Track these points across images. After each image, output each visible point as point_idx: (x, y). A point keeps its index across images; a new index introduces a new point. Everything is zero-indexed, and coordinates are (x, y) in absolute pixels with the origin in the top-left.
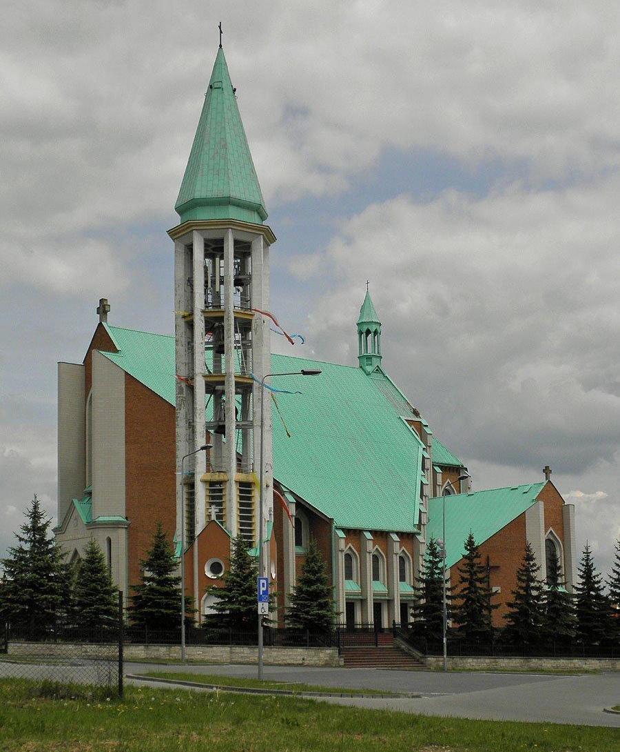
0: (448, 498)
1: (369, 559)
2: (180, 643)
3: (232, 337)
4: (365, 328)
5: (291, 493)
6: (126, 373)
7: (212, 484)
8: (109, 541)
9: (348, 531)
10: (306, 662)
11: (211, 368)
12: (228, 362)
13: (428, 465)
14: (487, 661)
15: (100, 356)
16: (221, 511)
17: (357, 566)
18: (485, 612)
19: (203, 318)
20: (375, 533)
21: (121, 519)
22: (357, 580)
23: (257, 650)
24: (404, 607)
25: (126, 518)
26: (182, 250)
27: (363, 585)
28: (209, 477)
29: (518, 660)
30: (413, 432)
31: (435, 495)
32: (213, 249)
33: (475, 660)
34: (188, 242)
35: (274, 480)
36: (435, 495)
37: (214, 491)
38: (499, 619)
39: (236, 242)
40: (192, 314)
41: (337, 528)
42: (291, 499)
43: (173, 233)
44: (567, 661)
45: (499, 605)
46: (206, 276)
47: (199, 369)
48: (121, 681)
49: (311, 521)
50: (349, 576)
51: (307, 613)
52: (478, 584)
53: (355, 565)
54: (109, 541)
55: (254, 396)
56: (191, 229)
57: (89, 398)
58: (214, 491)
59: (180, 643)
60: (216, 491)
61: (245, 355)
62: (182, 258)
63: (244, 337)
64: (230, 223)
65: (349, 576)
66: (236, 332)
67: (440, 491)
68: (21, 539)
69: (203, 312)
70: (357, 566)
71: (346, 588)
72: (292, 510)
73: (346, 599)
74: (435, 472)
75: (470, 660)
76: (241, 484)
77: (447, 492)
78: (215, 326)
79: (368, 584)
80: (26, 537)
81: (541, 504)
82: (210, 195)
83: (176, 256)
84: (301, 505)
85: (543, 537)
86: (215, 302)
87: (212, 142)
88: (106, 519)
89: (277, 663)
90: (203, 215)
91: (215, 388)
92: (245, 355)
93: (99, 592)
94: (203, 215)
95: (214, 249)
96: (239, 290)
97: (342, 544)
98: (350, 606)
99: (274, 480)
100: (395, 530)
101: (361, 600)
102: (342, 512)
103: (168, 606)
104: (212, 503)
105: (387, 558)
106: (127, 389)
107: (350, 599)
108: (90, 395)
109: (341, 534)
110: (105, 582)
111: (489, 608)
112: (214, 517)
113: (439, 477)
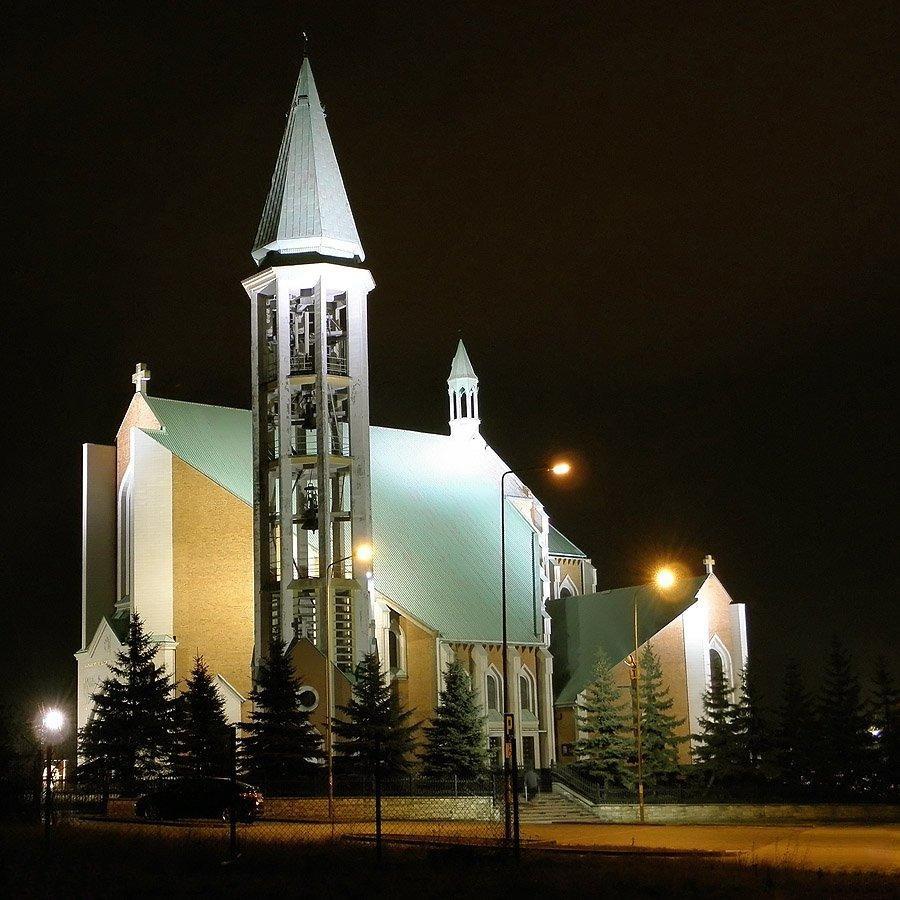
22: (534, 709)
59: (329, 796)
68: (119, 672)
80: (123, 668)
111: (675, 741)
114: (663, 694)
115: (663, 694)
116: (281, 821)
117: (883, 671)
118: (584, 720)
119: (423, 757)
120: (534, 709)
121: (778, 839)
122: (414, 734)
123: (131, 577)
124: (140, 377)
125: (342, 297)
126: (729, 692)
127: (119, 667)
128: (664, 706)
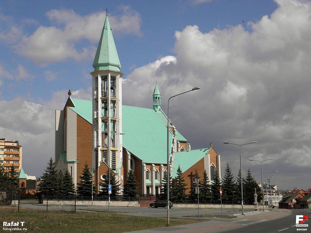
0: (182, 152)
1: (154, 173)
2: (91, 200)
3: (110, 105)
4: (155, 96)
5: (129, 152)
6: (77, 114)
7: (103, 151)
8: (71, 167)
9: (147, 164)
10: (129, 206)
11: (104, 115)
12: (108, 113)
13: (175, 141)
14: (184, 205)
15: (69, 108)
16: (106, 159)
17: (150, 175)
18: (184, 191)
19: (101, 100)
20: (156, 164)
21: (75, 160)
22: (150, 179)
23: (108, 202)
24: (157, 188)
25: (77, 160)
26: (94, 79)
27: (152, 181)
28: (102, 149)
29: (193, 205)
30: (170, 131)
31: (178, 151)
32: (104, 78)
33: (180, 205)
34: (96, 76)
35: (123, 147)
36: (178, 151)
37: (104, 153)
38: (187, 192)
39: (111, 76)
40: (98, 98)
41: (143, 163)
42: (129, 154)
43: (92, 73)
44: (209, 205)
45: (188, 189)
46: (102, 87)
47: (100, 116)
48: (75, 210)
49: (136, 161)
50: (147, 178)
51: (129, 191)
52: (181, 182)
53: (150, 174)
54: (71, 167)
55: (117, 123)
56: (97, 73)
57: (65, 121)
58: (104, 153)
59: (91, 200)
60: (105, 153)
61: (114, 111)
62: (94, 81)
63: (114, 105)
64: (109, 71)
65: (147, 178)
66: (111, 103)
67: (179, 150)
68: (47, 171)
69: (101, 98)
70: (150, 175)
71: (147, 182)
72: (129, 157)
73: (155, 185)
74: (178, 144)
75: (179, 205)
76: (112, 151)
77: (182, 150)
78: (105, 101)
79: (154, 181)
80: (48, 170)
81: (209, 155)
82: (103, 62)
83: (93, 80)
84: (132, 156)
85: (210, 165)
86: (105, 94)
87: (104, 46)
88: (71, 160)
89: (120, 206)
90: (101, 68)
91: (105, 121)
92: (114, 111)
93: (68, 186)
94: (101, 68)
95: (105, 79)
96: (112, 91)
97: (146, 168)
98: (148, 188)
99: (123, 147)
100: (162, 163)
101: (160, 186)
102: (145, 158)
103: (88, 190)
104: (104, 157)
105: (160, 172)
106: (77, 119)
107: (148, 185)
108: (65, 120)
109: (145, 165)
110: (71, 182)
111: (185, 189)
112: (104, 161)
113: (179, 145)
114: (182, 178)
115: (182, 178)
116: (71, 205)
117: (249, 173)
118: (163, 184)
119: (185, 189)
120: (150, 179)
121: (210, 214)
122: (120, 186)
123: (66, 138)
124: (24, 222)
125: (61, 171)
126: (120, 185)
127: (47, 170)
128: (182, 181)
